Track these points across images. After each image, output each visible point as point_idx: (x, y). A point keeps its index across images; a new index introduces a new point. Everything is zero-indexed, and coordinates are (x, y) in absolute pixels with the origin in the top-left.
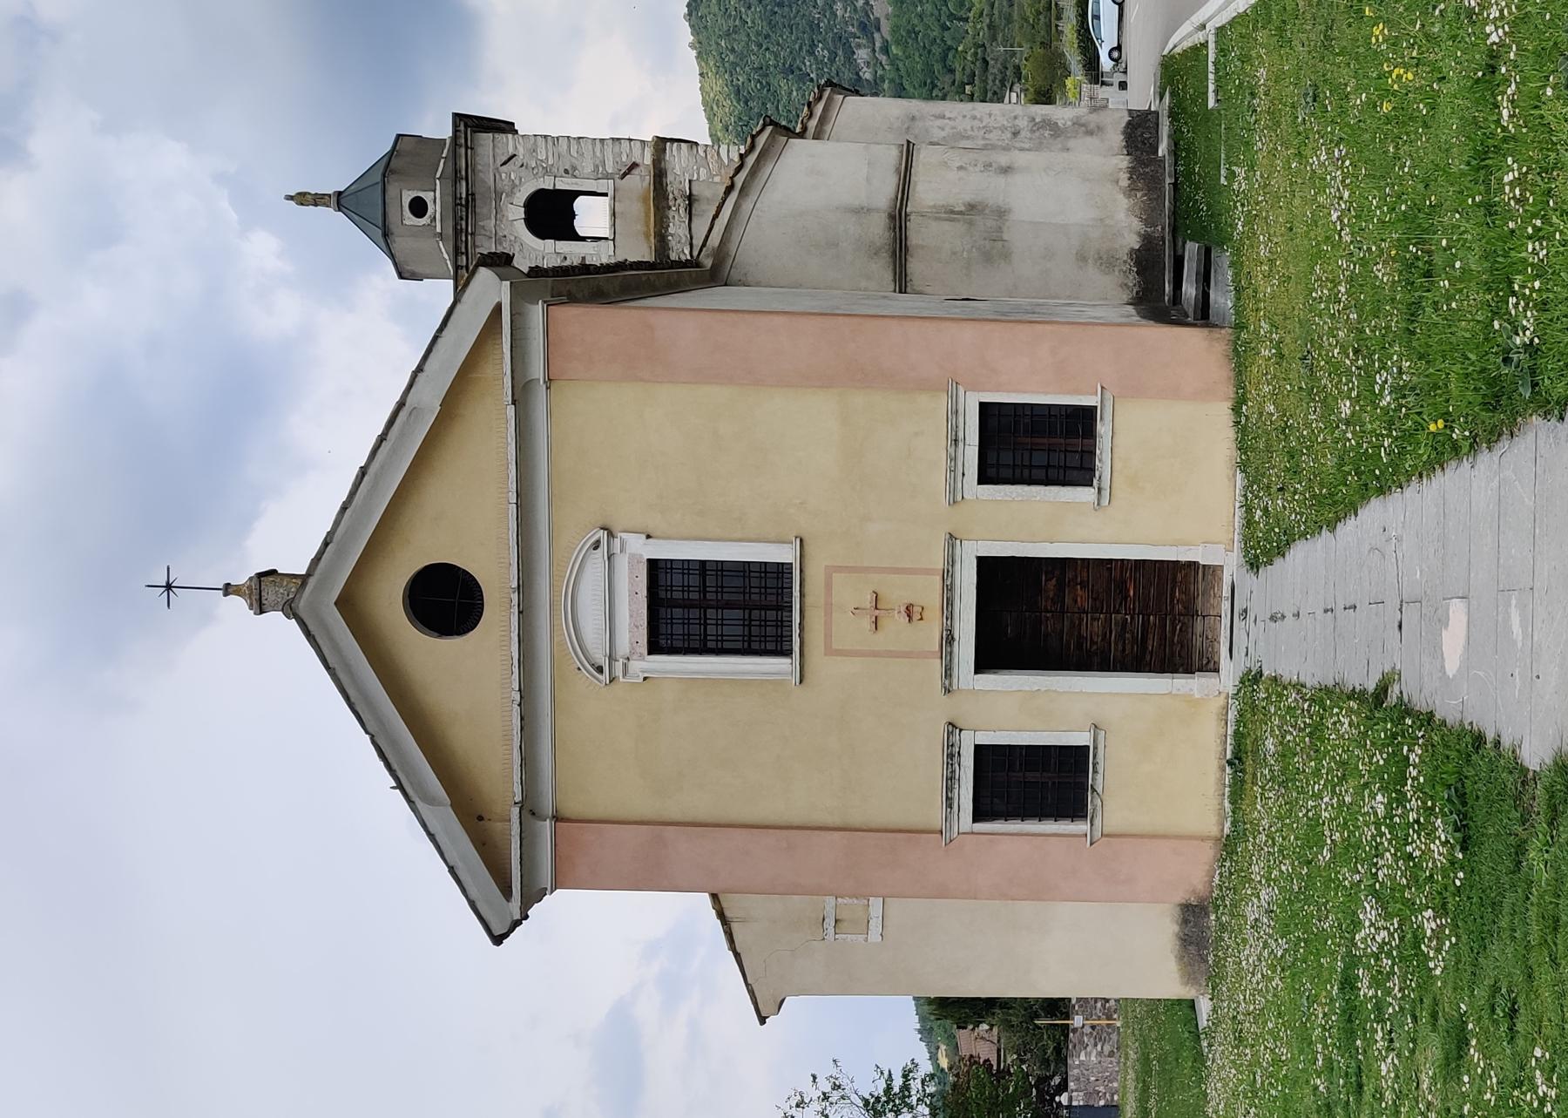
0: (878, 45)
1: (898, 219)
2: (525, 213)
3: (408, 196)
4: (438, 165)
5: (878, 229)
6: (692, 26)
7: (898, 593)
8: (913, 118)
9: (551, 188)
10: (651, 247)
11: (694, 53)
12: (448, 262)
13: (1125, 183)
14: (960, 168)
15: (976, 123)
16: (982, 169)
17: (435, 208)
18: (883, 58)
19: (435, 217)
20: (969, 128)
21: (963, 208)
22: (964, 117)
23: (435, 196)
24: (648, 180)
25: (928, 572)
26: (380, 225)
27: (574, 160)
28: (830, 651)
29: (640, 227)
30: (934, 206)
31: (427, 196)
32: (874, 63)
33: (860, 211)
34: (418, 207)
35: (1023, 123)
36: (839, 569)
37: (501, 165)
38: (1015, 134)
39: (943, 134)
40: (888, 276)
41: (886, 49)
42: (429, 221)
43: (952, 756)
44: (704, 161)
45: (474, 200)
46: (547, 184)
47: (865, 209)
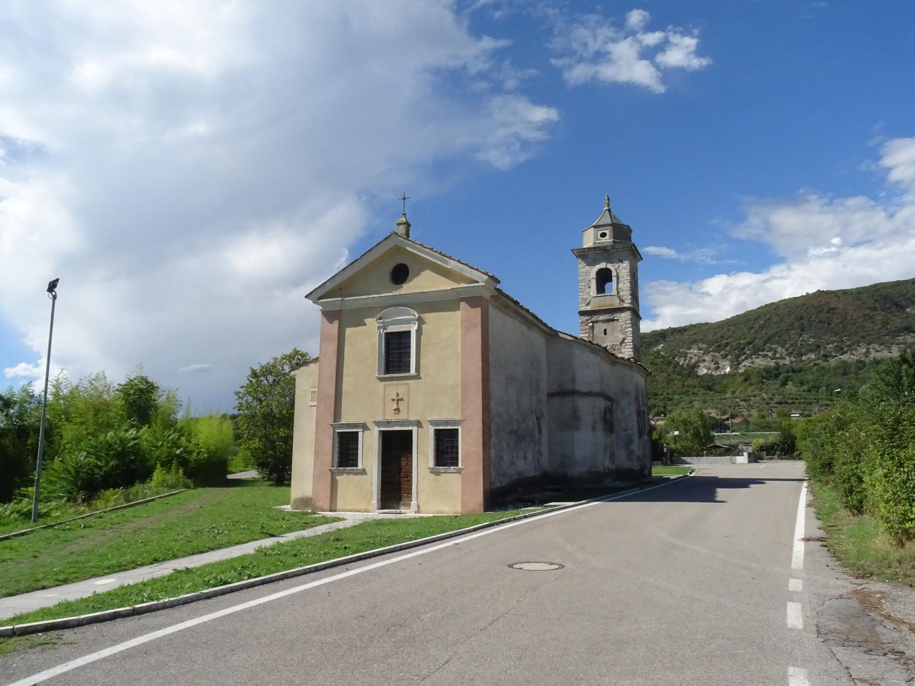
0: (817, 361)
1: (572, 393)
3: (607, 232)
5: (569, 387)
6: (815, 293)
7: (402, 405)
11: (804, 294)
13: (592, 470)
17: (603, 240)
18: (811, 364)
25: (408, 414)
28: (385, 386)
31: (607, 237)
32: (810, 360)
33: (573, 380)
34: (603, 235)
35: (630, 432)
36: (409, 387)
38: (626, 430)
41: (816, 365)
43: (355, 425)
46: (614, 274)
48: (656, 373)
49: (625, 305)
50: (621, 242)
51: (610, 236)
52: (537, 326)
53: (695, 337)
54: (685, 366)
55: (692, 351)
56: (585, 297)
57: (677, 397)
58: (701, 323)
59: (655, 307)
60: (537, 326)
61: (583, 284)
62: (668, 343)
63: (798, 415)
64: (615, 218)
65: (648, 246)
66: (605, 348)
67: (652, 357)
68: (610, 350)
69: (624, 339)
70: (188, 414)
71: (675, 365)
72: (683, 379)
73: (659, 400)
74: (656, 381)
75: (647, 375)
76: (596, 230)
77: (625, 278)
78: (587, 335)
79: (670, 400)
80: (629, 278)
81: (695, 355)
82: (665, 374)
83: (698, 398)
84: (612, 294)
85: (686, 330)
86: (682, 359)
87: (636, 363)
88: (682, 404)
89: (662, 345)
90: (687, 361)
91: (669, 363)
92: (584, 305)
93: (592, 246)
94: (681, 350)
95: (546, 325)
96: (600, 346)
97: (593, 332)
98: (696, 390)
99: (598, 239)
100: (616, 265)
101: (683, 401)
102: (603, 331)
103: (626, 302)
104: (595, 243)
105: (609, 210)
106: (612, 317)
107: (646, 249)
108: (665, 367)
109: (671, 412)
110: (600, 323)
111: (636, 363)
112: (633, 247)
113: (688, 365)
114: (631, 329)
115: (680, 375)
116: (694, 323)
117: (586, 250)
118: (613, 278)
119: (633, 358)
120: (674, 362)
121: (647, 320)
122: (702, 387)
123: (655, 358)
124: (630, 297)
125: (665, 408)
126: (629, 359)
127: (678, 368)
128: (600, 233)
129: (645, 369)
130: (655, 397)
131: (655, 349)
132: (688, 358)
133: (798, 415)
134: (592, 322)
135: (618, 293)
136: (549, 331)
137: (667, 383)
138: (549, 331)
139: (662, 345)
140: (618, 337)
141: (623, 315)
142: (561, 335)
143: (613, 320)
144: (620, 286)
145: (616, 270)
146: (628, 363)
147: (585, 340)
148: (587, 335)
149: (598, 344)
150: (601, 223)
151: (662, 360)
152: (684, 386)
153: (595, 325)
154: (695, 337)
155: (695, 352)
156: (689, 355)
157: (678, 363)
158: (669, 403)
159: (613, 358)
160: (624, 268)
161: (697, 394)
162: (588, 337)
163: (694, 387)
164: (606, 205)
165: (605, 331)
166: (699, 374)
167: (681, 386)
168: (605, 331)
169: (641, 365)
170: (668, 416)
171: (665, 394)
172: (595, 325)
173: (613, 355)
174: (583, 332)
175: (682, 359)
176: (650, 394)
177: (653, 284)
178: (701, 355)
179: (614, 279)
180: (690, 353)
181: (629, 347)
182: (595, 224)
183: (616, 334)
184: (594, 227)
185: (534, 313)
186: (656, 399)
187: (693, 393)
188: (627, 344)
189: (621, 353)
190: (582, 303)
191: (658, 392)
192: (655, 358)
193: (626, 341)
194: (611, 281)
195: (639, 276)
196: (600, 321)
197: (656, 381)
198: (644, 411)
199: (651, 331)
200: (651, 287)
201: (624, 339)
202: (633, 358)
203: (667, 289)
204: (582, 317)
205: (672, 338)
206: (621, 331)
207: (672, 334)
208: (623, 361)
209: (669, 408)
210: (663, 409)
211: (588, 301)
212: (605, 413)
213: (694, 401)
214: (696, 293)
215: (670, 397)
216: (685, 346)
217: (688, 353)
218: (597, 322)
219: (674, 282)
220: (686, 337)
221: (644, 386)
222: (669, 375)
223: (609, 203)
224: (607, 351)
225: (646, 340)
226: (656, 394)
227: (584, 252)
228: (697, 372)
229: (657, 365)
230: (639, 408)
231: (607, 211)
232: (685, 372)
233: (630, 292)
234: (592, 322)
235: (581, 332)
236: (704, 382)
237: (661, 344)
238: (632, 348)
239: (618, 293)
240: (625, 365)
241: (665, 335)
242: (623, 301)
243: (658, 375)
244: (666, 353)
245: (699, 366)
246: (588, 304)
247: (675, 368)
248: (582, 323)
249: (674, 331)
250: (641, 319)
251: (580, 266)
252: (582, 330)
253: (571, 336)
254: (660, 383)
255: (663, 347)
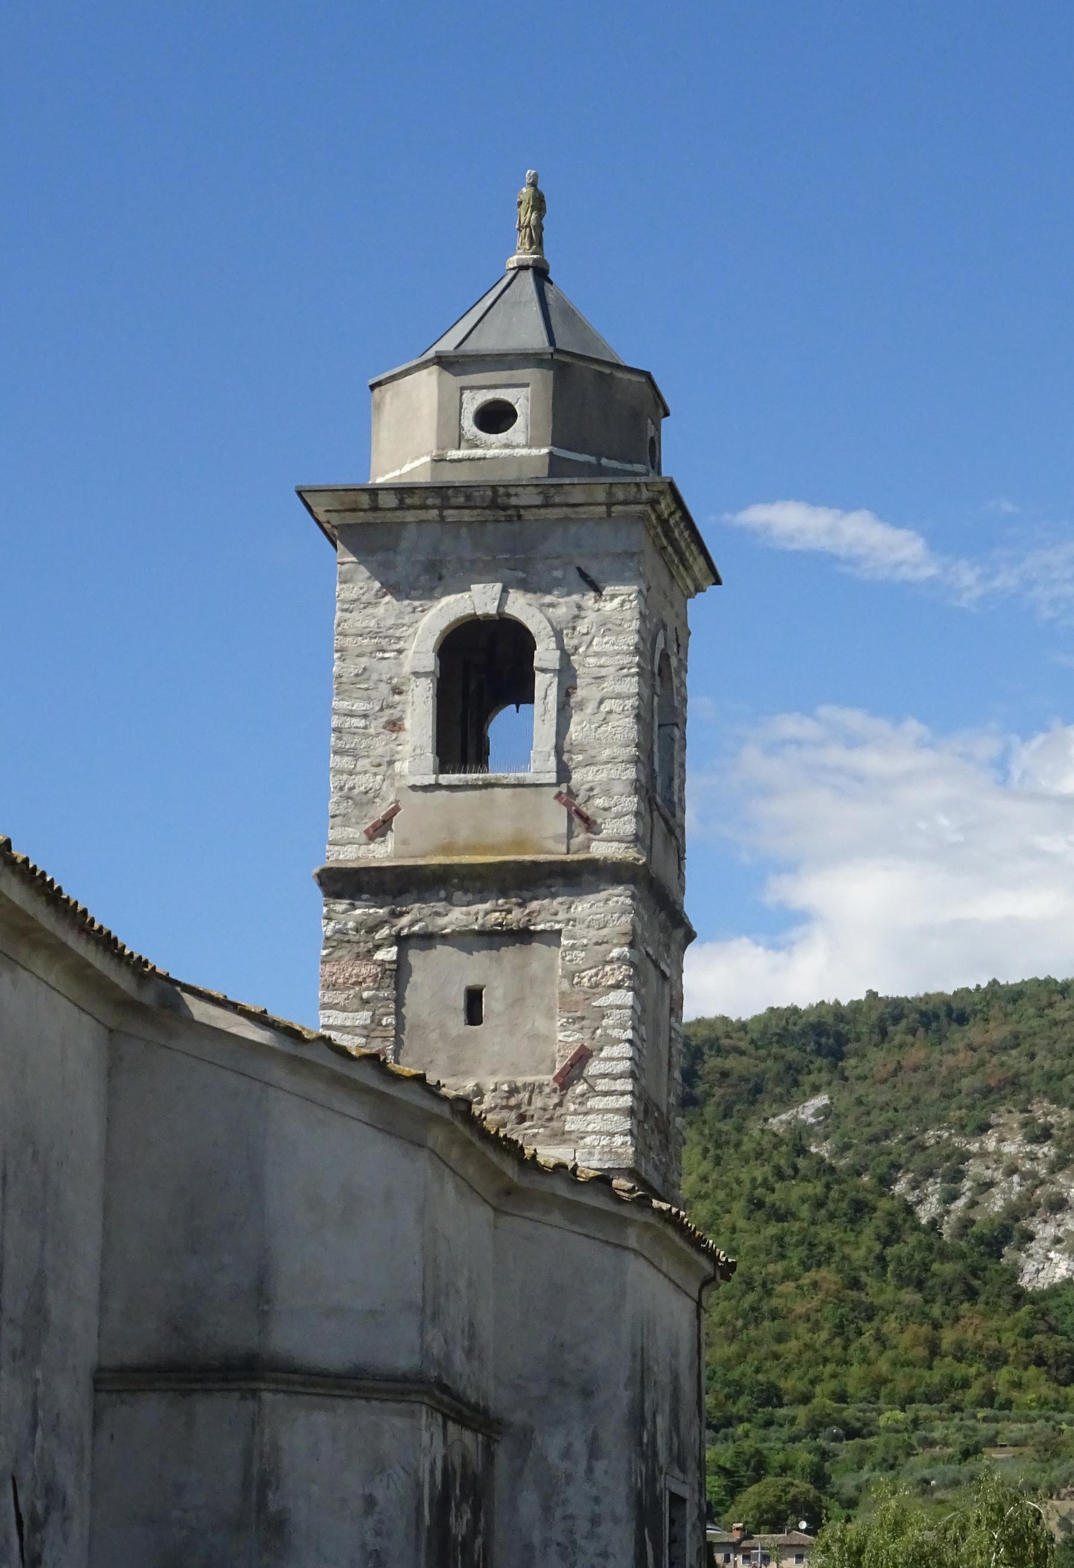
2: (486, 616)
3: (520, 399)
4: (581, 451)
8: (587, 1393)
9: (536, 664)
10: (423, 856)
12: (397, 473)
14: (370, 1502)
15: (583, 1526)
16: (369, 1548)
19: (477, 446)
20: (570, 1510)
21: (273, 1508)
22: (597, 1500)
23: (518, 446)
24: (557, 852)
26: (469, 347)
27: (590, 708)
29: (464, 834)
30: (276, 1449)
31: (517, 432)
37: (579, 569)
39: (553, 1456)
40: (131, 1355)
42: (469, 436)
44: (600, 958)
45: (509, 520)
46: (545, 654)
47: (266, 1307)
48: (779, 1267)
49: (600, 850)
50: (600, 471)
51: (534, 423)
52: (58, 950)
53: (1015, 1059)
54: (946, 1230)
55: (991, 1145)
56: (363, 782)
57: (891, 1416)
58: (1049, 982)
59: (790, 867)
60: (58, 950)
61: (359, 706)
62: (860, 1089)
63: (639, 1486)
64: (569, 313)
65: (770, 497)
66: (462, 1107)
67: (760, 1172)
68: (491, 1121)
69: (583, 1057)
70: (369, 578)
71: (893, 1226)
72: (936, 1311)
73: (786, 1432)
74: (774, 1315)
75: (707, 1282)
76: (454, 382)
77: (608, 686)
78: (363, 1017)
79: (852, 1433)
80: (632, 685)
81: (1012, 1171)
82: (828, 1276)
83: (1016, 1429)
84: (529, 777)
85: (962, 1019)
86: (934, 1188)
87: (643, 1203)
88: (919, 1464)
89: (821, 1100)
90: (961, 1203)
91: (860, 1209)
92: (355, 833)
93: (424, 478)
94: (930, 1137)
95: (107, 943)
96: (433, 1091)
97: (399, 1002)
98: (1003, 1376)
99: (460, 440)
100: (563, 607)
101: (930, 1443)
102: (461, 1002)
103: (609, 827)
104: (439, 460)
105: (541, 273)
106: (516, 917)
107: (757, 515)
108: (826, 1233)
109: (851, 1504)
110: (442, 951)
111: (643, 1203)
112: (665, 505)
113: (966, 1224)
114: (627, 997)
115: (920, 1285)
116: (1011, 977)
117: (388, 500)
118: (540, 680)
119: (631, 1173)
120: (884, 1204)
121: (745, 940)
122: (1040, 1361)
123: (780, 1175)
124: (632, 802)
125: (819, 1479)
126: (603, 1180)
127: (907, 1246)
128: (474, 401)
129: (697, 1243)
130: (763, 1413)
131: (778, 1123)
132: (967, 1184)
133: (639, 1486)
134: (401, 941)
135: (564, 773)
136: (124, 981)
137: (840, 1328)
138: (124, 981)
139: (821, 1100)
140: (548, 1039)
141: (584, 907)
142: (200, 1011)
143: (523, 936)
144: (575, 732)
145: (558, 635)
146: (599, 1202)
147: (342, 1052)
148: (363, 1017)
149: (420, 1079)
150: (486, 342)
151: (815, 1188)
152: (934, 1349)
153: (415, 957)
154: (1015, 1059)
155: (1009, 1148)
156: (974, 1168)
157: (909, 1210)
158: (846, 1450)
159: (510, 1169)
160: (606, 626)
161: (1008, 1405)
162: (368, 1032)
163: (997, 1360)
164: (522, 240)
165: (474, 998)
166: (1024, 1282)
167: (921, 1352)
168: (474, 998)
169: (673, 1220)
170: (833, 1529)
171: (822, 1400)
172: (415, 957)
173: (513, 1149)
174: (340, 998)
175: (934, 1188)
176: (737, 1390)
177: (790, 726)
178: (1043, 1172)
179: (545, 686)
180: (983, 1154)
181: (611, 1102)
182: (447, 345)
183: (541, 1024)
184: (443, 362)
185: (39, 862)
186: (768, 1423)
187: (989, 1399)
188: (602, 1085)
189: (561, 1137)
190: (346, 820)
191: (783, 1384)
192: (780, 1175)
193: (594, 1067)
194: (524, 694)
195: (693, 679)
196: (445, 939)
197: (774, 1315)
198: (677, 1500)
199: (761, 1010)
200: (774, 748)
201: (583, 1057)
202: (631, 1173)
203: (871, 761)
204: (341, 906)
205: (879, 1059)
206: (566, 1003)
207: (884, 1033)
208: (562, 1189)
209: (845, 1482)
210: (802, 1486)
211: (380, 811)
212: (442, 1504)
213: (992, 1442)
214: (1042, 797)
215: (850, 1412)
216: (954, 1114)
217: (965, 1156)
218: (428, 939)
219: (913, 726)
220: (965, 1059)
221: (685, 1349)
222: (855, 1284)
223: (539, 227)
224: (474, 1122)
225: (731, 1063)
226: (772, 1396)
227: (375, 508)
228: (1015, 1272)
229: (780, 1216)
230: (651, 1480)
231: (528, 277)
232: (948, 1269)
233: (631, 773)
234: (401, 941)
235: (329, 997)
236: (1052, 1330)
237: (816, 1090)
238: (631, 1112)
239: (564, 773)
240: (573, 1210)
241: (841, 1039)
242: (590, 824)
243: (787, 1276)
244: (844, 1148)
245: (1030, 1237)
246: (380, 829)
247: (887, 1242)
248: (338, 941)
249: (896, 1020)
250: (690, 936)
251: (346, 592)
252: (332, 986)
253: (260, 1019)
254: (802, 1328)
255: (825, 1112)
